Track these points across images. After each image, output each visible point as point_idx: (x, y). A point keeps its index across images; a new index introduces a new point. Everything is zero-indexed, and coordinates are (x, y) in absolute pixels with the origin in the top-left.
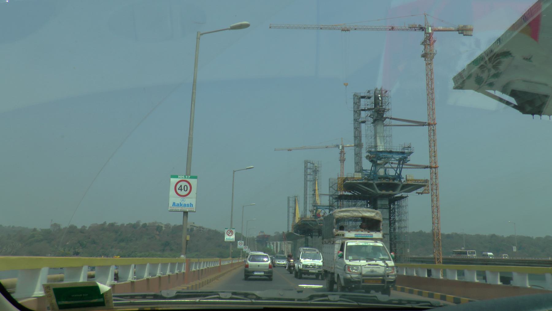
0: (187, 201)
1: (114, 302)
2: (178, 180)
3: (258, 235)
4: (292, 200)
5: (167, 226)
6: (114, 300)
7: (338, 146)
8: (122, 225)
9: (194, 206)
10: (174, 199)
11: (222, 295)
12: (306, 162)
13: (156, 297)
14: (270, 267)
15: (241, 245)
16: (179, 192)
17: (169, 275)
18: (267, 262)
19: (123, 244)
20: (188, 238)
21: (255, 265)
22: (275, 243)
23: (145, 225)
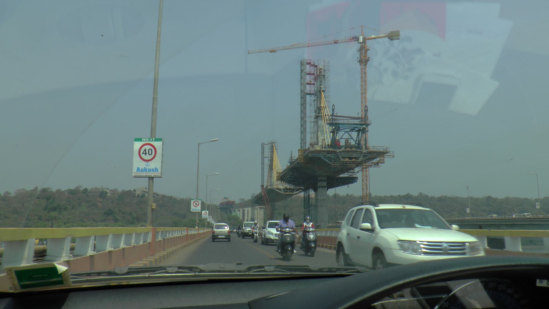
0: (153, 165)
1: (71, 280)
2: (143, 143)
3: (221, 202)
5: (114, 192)
6: (72, 278)
8: (58, 191)
9: (159, 171)
10: (137, 163)
11: (169, 270)
13: (110, 273)
14: (229, 232)
15: (205, 214)
16: (143, 156)
17: (123, 249)
18: (227, 229)
19: (53, 214)
20: (154, 206)
21: (219, 232)
22: (241, 210)
23: (86, 190)
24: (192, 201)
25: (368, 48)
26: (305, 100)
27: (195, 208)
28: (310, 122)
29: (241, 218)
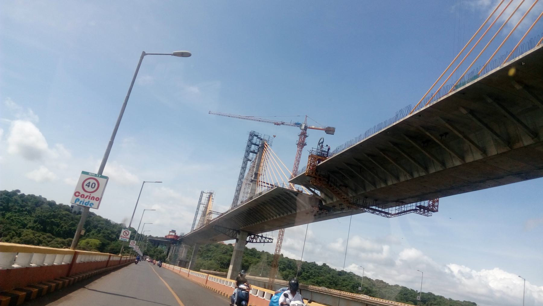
4: (205, 196)
7: (298, 125)
12: (253, 135)
16: (86, 188)
24: (123, 230)
25: (307, 135)
26: (246, 164)
27: (124, 236)
28: (246, 184)
29: (165, 253)
